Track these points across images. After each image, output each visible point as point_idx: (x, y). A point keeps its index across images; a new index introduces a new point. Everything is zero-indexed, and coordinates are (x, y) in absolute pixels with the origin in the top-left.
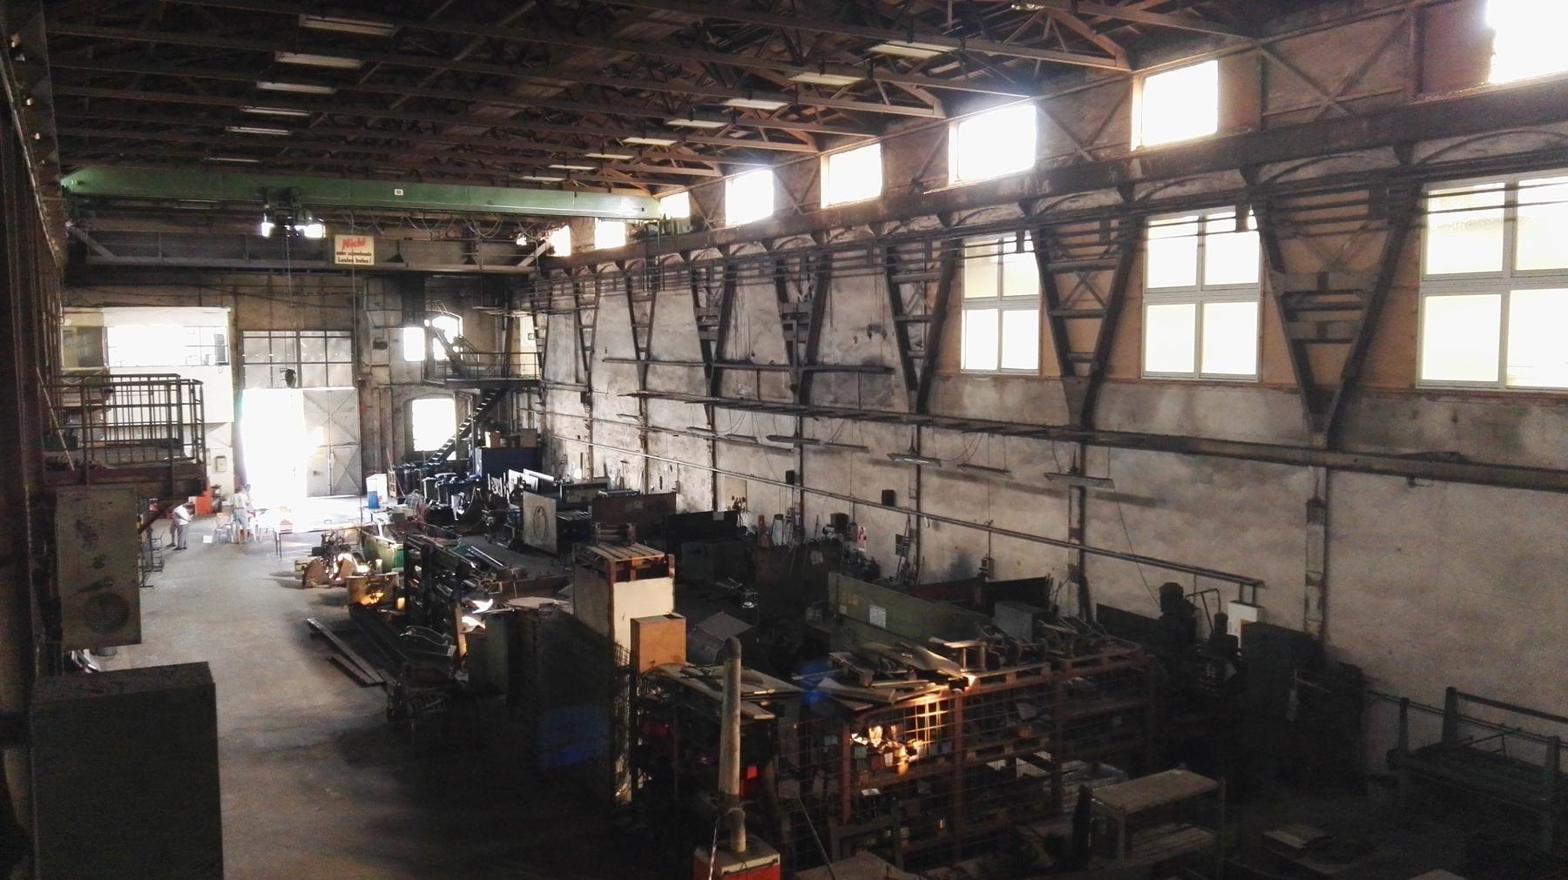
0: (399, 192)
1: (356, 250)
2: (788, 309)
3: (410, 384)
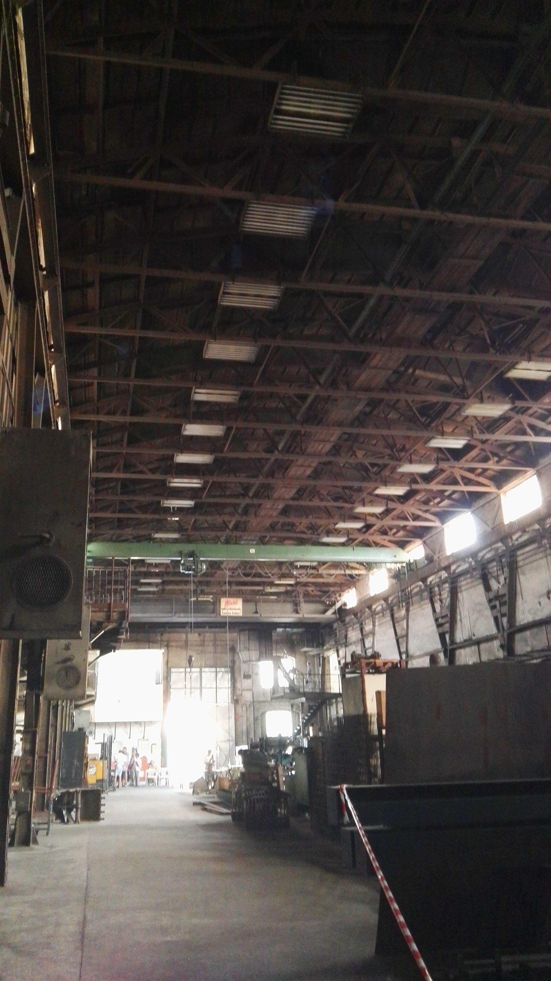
0: (253, 551)
2: (492, 595)
3: (264, 702)
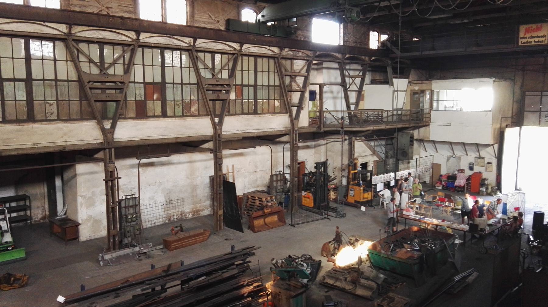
1: (535, 34)
